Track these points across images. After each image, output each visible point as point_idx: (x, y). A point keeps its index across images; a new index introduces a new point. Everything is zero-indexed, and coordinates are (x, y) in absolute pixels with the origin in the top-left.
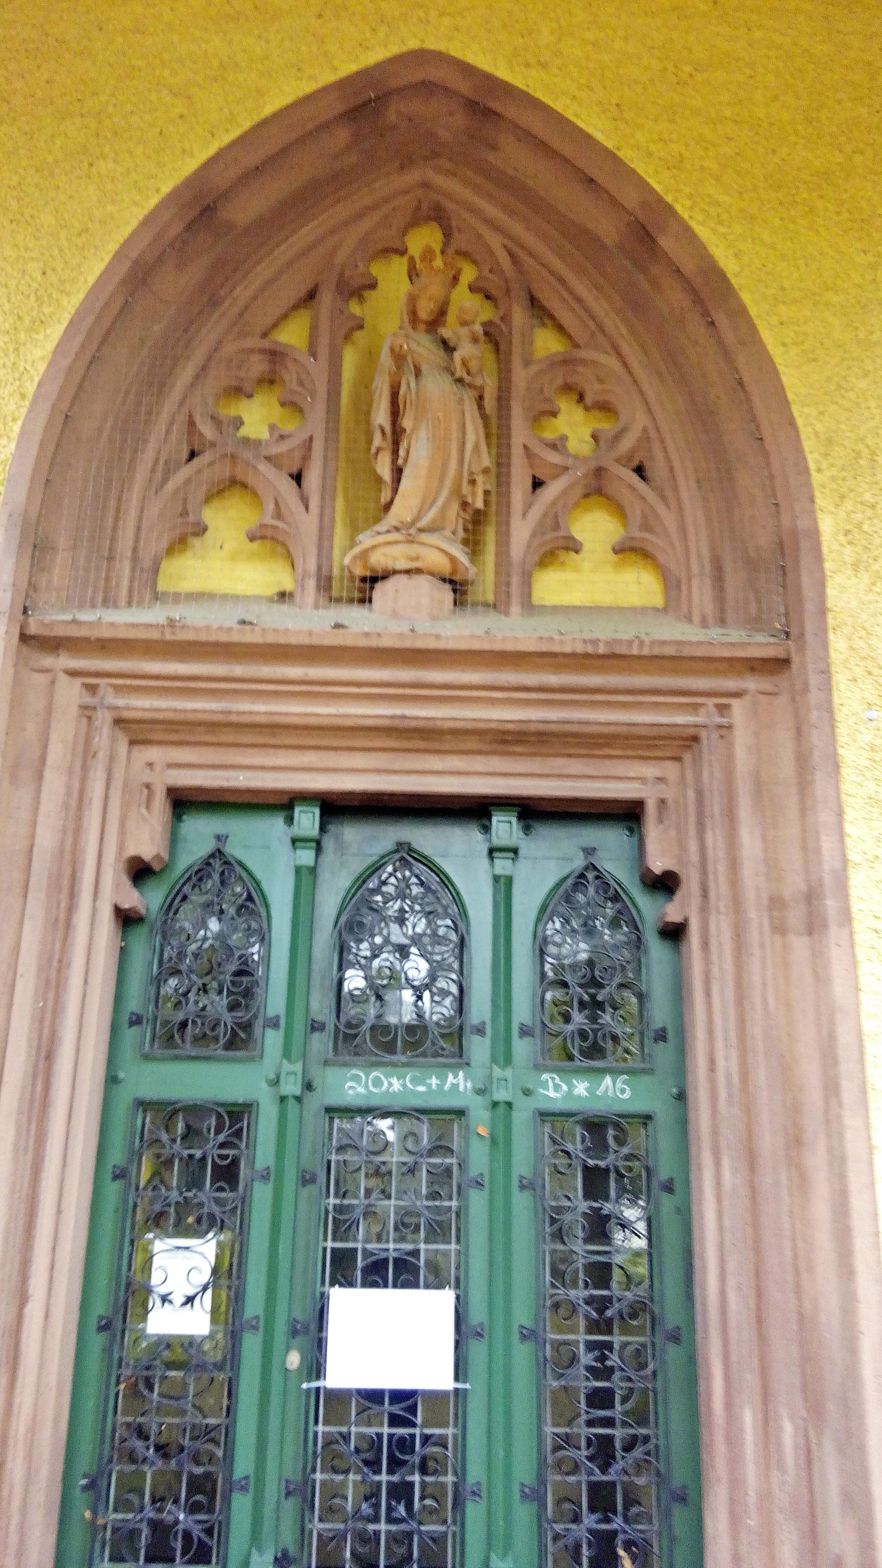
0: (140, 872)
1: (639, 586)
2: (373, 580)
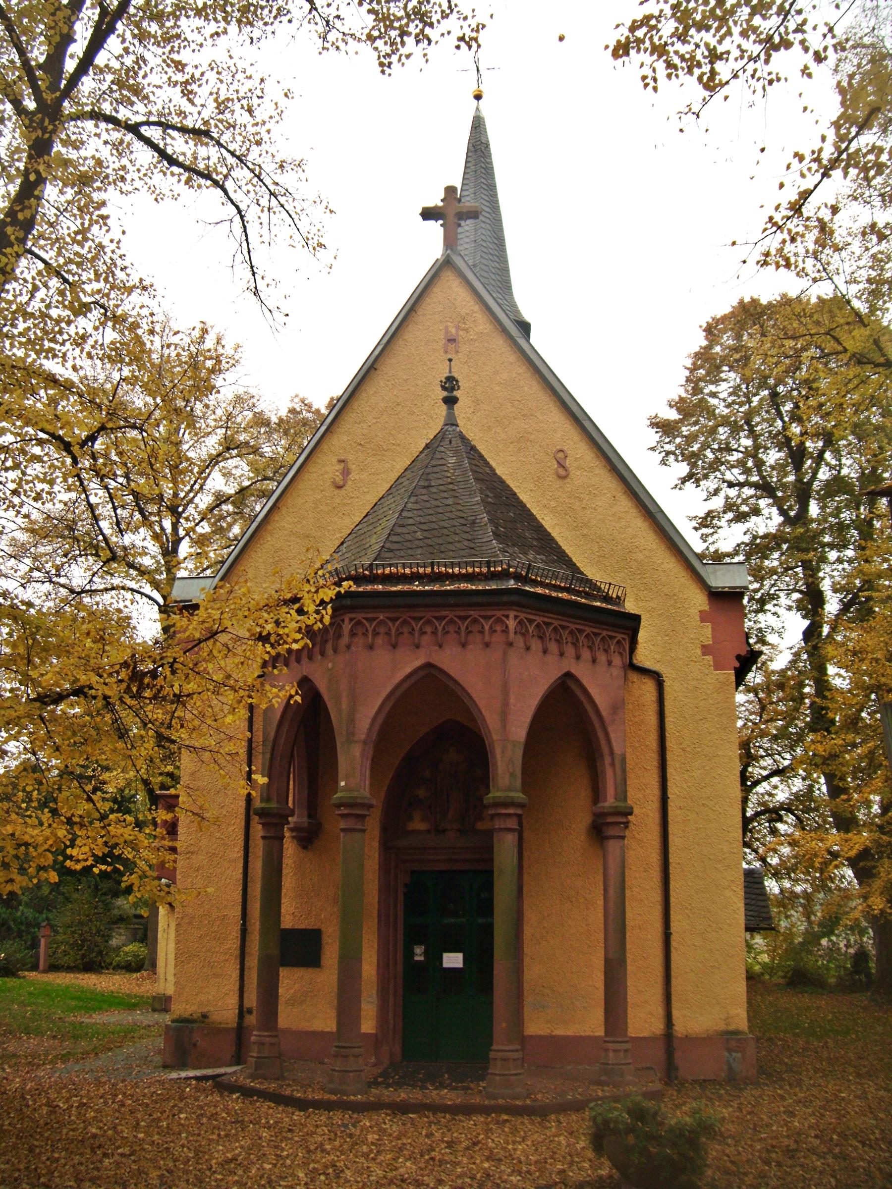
0: (406, 885)
2: (444, 831)
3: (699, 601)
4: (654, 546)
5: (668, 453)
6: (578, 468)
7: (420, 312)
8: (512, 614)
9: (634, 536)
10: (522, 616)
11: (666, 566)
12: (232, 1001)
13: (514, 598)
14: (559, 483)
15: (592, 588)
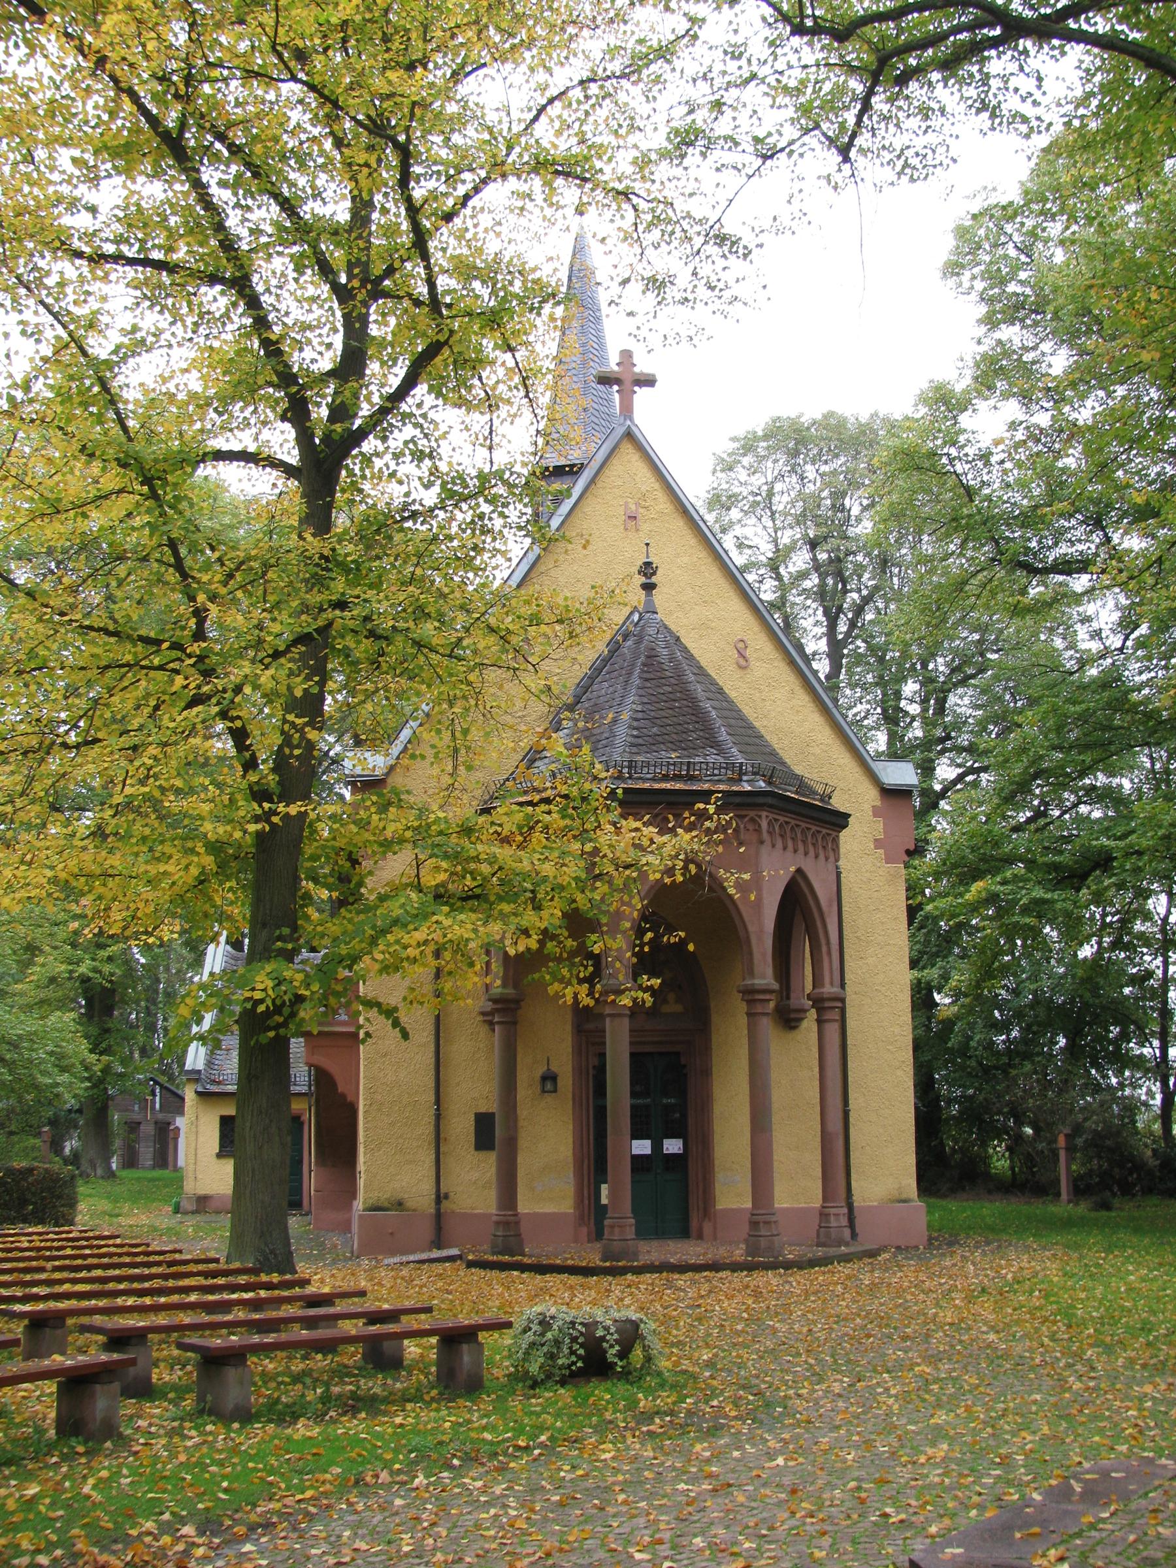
1: (678, 1008)
3: (871, 796)
4: (830, 741)
5: (145, 297)
6: (758, 659)
7: (600, 484)
8: (764, 814)
9: (812, 730)
10: (771, 816)
11: (841, 761)
12: (428, 1187)
13: (769, 800)
14: (740, 673)
15: (801, 784)
